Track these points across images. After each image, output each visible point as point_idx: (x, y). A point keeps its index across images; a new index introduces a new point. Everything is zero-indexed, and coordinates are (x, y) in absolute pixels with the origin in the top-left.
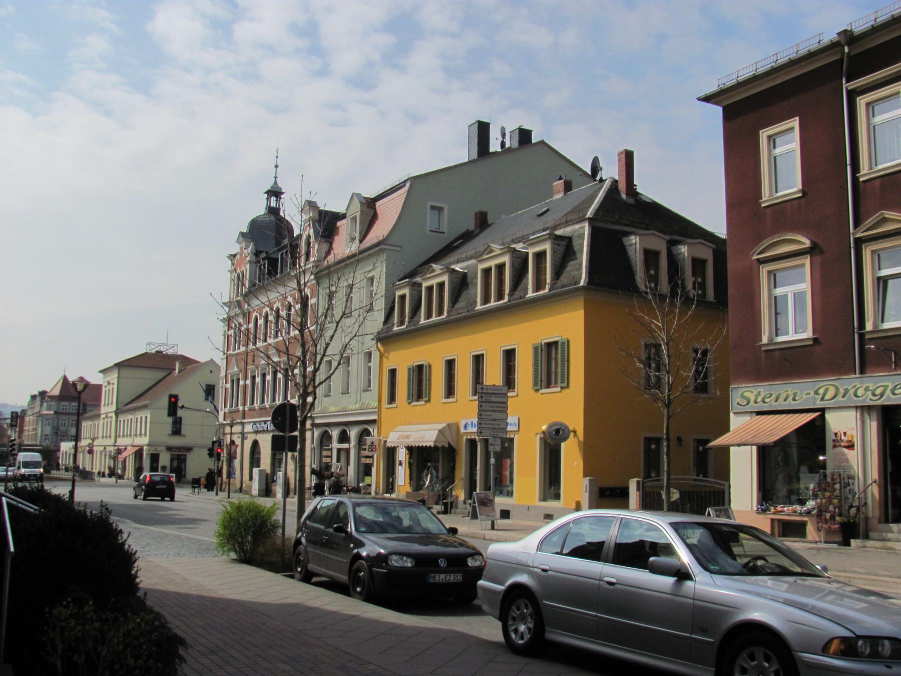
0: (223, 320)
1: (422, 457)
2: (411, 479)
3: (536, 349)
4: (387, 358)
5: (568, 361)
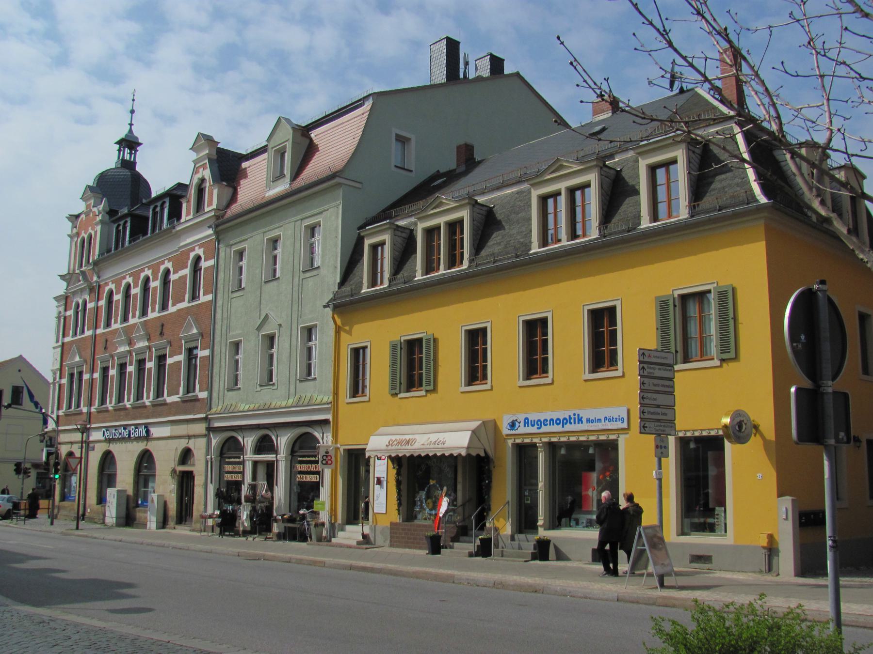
0: (57, 299)
1: (418, 474)
2: (400, 504)
3: (394, 347)
4: (349, 332)
5: (735, 318)
